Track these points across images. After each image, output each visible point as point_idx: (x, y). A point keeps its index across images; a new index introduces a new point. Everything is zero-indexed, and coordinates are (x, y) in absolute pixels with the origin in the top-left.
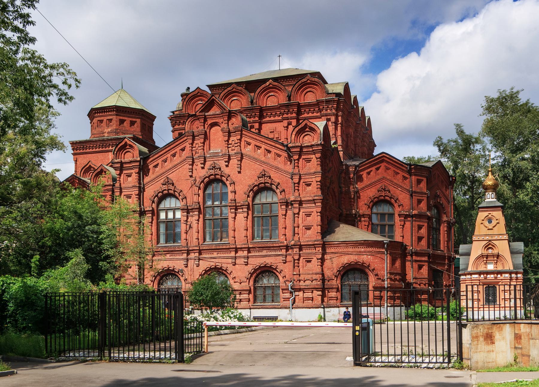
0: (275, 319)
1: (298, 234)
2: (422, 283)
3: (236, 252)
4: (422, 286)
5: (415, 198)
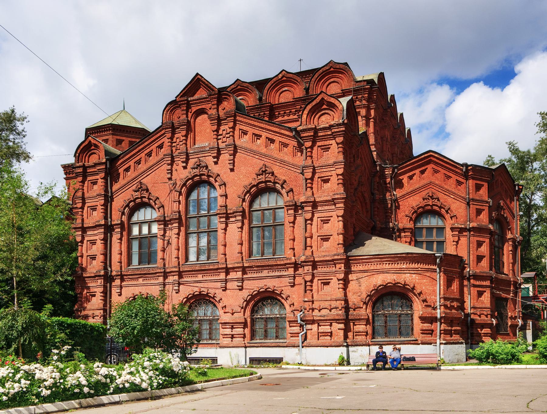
0: (277, 361)
1: (311, 247)
2: (483, 314)
3: (227, 273)
4: (483, 317)
5: (473, 208)
